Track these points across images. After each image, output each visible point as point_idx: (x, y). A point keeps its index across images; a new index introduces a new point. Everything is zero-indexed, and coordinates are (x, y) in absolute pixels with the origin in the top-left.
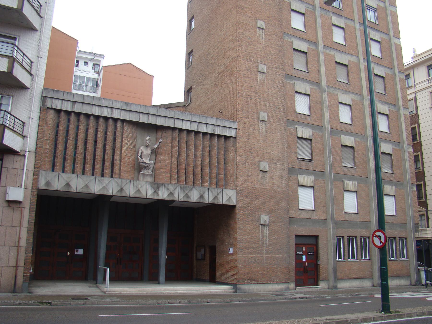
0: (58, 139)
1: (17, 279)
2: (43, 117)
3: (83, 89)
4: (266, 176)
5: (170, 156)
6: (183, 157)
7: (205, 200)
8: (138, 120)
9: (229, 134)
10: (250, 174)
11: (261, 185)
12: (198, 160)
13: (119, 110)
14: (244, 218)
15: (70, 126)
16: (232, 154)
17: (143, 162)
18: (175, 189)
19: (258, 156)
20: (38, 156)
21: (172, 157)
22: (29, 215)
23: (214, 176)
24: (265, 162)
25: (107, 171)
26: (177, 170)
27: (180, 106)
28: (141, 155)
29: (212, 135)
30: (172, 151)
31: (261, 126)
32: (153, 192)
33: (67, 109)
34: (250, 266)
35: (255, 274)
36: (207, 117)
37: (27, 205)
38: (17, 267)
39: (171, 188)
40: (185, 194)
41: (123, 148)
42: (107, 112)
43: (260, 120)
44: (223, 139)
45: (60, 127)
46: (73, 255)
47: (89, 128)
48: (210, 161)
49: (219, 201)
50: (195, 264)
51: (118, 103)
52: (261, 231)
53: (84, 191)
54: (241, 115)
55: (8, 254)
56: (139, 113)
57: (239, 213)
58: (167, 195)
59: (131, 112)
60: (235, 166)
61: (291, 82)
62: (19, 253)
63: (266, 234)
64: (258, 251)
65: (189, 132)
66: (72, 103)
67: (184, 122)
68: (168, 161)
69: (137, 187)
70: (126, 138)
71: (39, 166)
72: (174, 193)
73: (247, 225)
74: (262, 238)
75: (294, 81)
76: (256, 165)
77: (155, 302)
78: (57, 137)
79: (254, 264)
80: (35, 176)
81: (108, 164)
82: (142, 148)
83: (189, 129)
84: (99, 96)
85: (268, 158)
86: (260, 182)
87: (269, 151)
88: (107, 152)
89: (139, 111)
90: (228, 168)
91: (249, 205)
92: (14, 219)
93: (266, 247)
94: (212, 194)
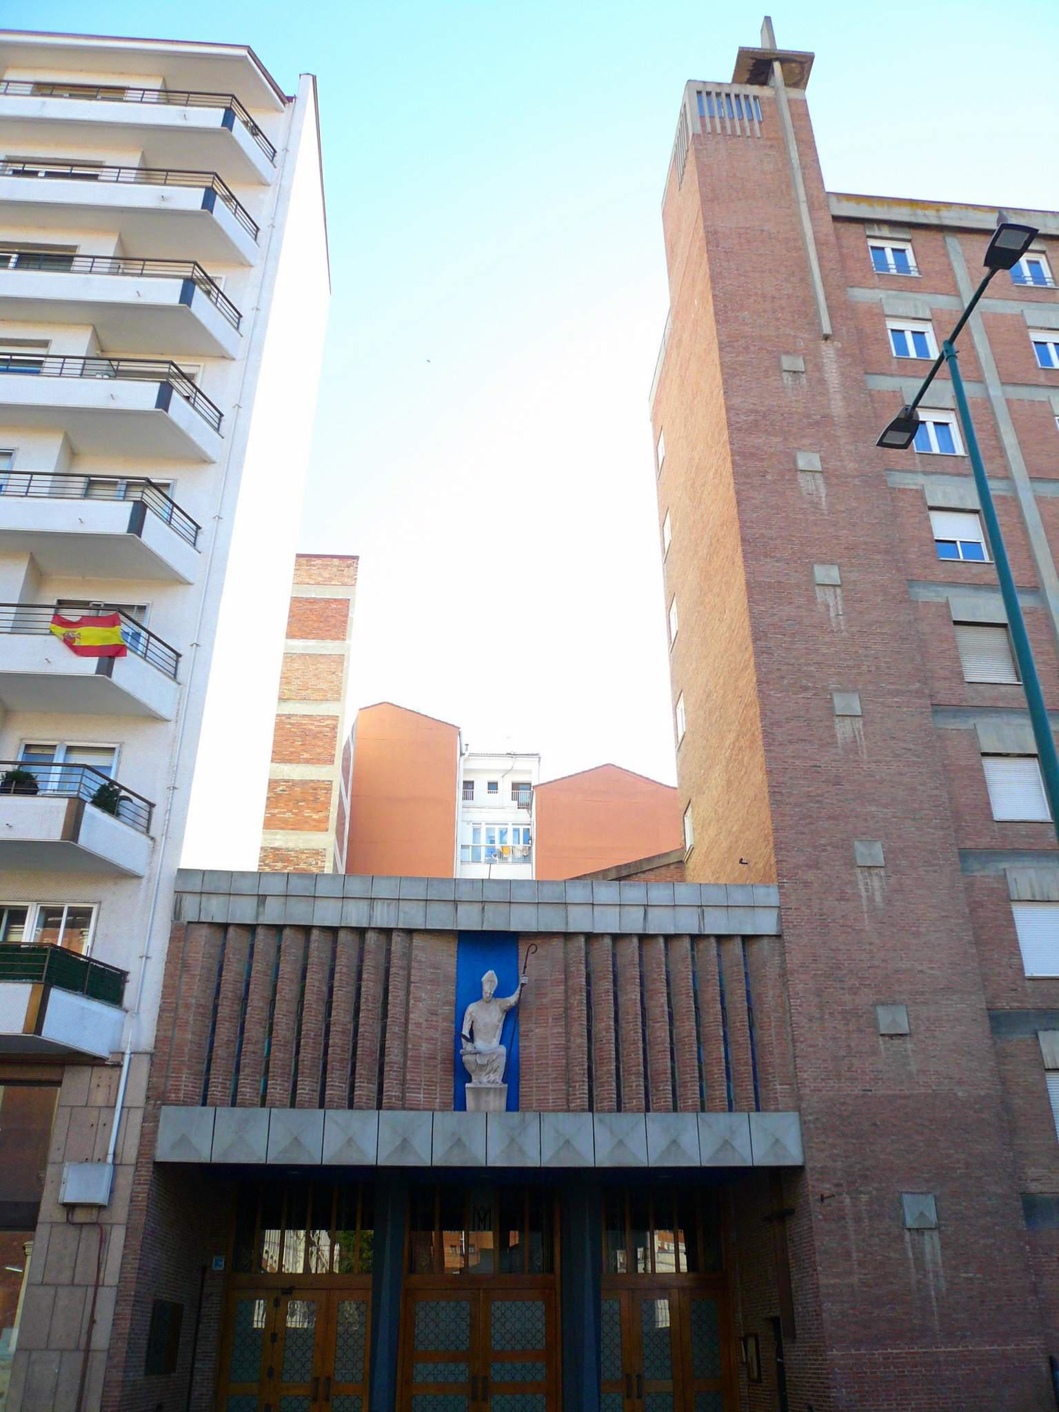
10: (842, 1053)
26: (586, 1067)
28: (471, 1032)
31: (867, 884)
60: (789, 1029)
61: (963, 727)
74: (919, 1282)
75: (972, 721)
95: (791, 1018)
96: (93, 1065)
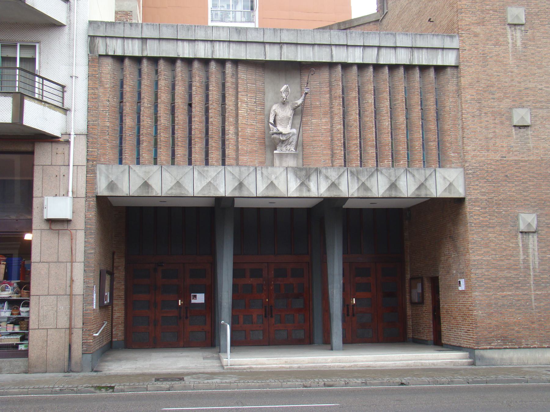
0: (124, 108)
1: (72, 349)
2: (94, 73)
3: (230, 18)
4: (527, 135)
5: (329, 116)
6: (354, 116)
7: (401, 192)
8: (262, 58)
9: (443, 60)
10: (490, 136)
11: (516, 155)
12: (383, 118)
13: (226, 44)
14: (482, 221)
15: (142, 82)
16: (451, 100)
17: (276, 133)
18: (340, 176)
19: (507, 98)
20: (91, 140)
21: (332, 118)
22: (85, 241)
23: (418, 144)
24: (523, 107)
25: (215, 155)
26: (342, 142)
27: (369, 23)
28: (275, 121)
29: (408, 68)
30: (331, 108)
31: (512, 35)
32: (299, 184)
33: (133, 53)
34: (501, 313)
35: (513, 330)
36: (394, 35)
37: (80, 224)
38: (70, 328)
39: (333, 174)
40: (360, 184)
41: (239, 111)
42: (205, 50)
43: (509, 24)
44: (432, 73)
45: (125, 86)
46: (188, 304)
47: (176, 82)
48: (407, 119)
49: (428, 193)
50: (409, 312)
51: (223, 31)
52: (521, 245)
53: (176, 192)
54: (467, 19)
55: (55, 309)
56: (263, 43)
57: (472, 212)
58: (325, 189)
59: (248, 45)
60: (460, 122)
62: (73, 306)
63: (534, 250)
64: (516, 285)
65: (362, 67)
66: (140, 41)
67: (350, 49)
69: (268, 179)
70: (243, 93)
71: (95, 156)
72: (339, 184)
73: (490, 235)
76: (503, 115)
77: (299, 382)
78: (121, 104)
79: (510, 310)
80: (89, 175)
81: (215, 143)
82: (275, 107)
83: (362, 62)
84: (257, 27)
85: (529, 99)
86: (514, 149)
87: (531, 85)
88: (212, 121)
89: (261, 40)
90: (446, 127)
91: (493, 195)
92: (60, 249)
93: (535, 276)
94: (415, 179)
95: (462, 115)
96: (52, 142)
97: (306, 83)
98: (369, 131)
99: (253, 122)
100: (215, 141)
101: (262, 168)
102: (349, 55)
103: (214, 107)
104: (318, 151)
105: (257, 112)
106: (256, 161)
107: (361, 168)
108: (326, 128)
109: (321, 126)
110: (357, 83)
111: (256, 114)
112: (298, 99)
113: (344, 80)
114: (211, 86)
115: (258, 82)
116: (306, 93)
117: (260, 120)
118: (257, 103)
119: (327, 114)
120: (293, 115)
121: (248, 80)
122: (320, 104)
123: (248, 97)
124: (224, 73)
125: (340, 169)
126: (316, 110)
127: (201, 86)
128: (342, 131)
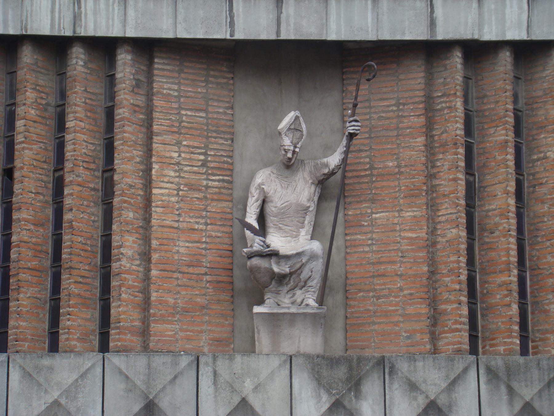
5: (423, 200)
18: (453, 384)
26: (464, 278)
28: (262, 218)
32: (327, 406)
40: (518, 406)
41: (155, 191)
42: (53, 11)
68: (411, 230)
69: (233, 390)
70: (167, 138)
72: (450, 406)
82: (261, 177)
88: (71, 222)
97: (351, 106)
98: (548, 243)
99: (197, 223)
100: (81, 280)
101: (215, 358)
102: (486, 16)
103: (80, 179)
104: (390, 305)
105: (210, 191)
106: (204, 337)
107: (521, 360)
108: (414, 235)
109: (400, 231)
110: (509, 100)
111: (206, 197)
112: (329, 150)
113: (473, 92)
114: (70, 117)
115: (215, 104)
116: (351, 136)
117: (218, 216)
118: (209, 164)
119: (416, 196)
120: (316, 199)
121: (182, 100)
122: (399, 166)
123: (182, 149)
124: (111, 80)
125: (452, 360)
126: (384, 184)
127: (43, 118)
128: (464, 246)
